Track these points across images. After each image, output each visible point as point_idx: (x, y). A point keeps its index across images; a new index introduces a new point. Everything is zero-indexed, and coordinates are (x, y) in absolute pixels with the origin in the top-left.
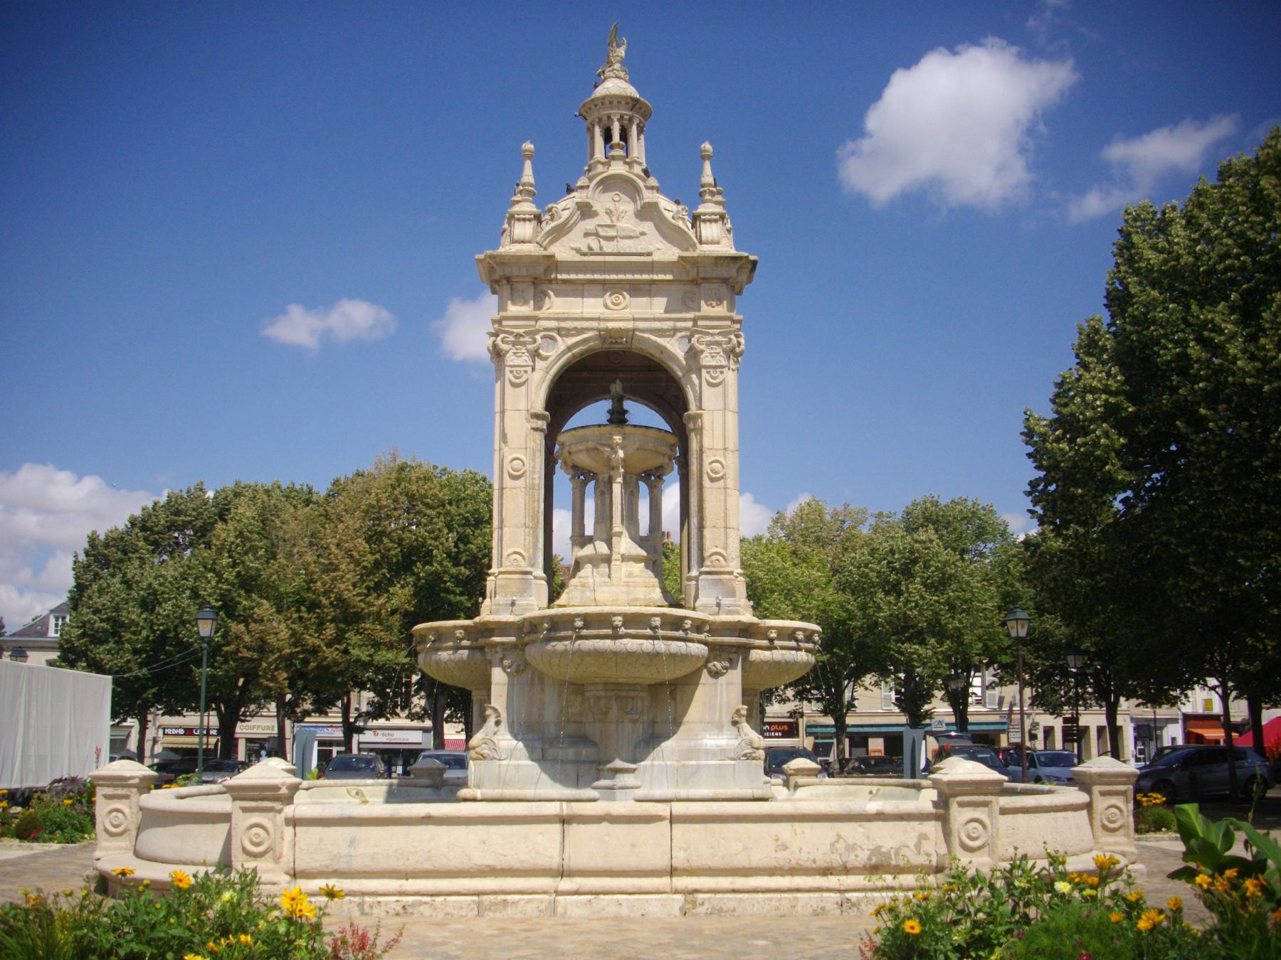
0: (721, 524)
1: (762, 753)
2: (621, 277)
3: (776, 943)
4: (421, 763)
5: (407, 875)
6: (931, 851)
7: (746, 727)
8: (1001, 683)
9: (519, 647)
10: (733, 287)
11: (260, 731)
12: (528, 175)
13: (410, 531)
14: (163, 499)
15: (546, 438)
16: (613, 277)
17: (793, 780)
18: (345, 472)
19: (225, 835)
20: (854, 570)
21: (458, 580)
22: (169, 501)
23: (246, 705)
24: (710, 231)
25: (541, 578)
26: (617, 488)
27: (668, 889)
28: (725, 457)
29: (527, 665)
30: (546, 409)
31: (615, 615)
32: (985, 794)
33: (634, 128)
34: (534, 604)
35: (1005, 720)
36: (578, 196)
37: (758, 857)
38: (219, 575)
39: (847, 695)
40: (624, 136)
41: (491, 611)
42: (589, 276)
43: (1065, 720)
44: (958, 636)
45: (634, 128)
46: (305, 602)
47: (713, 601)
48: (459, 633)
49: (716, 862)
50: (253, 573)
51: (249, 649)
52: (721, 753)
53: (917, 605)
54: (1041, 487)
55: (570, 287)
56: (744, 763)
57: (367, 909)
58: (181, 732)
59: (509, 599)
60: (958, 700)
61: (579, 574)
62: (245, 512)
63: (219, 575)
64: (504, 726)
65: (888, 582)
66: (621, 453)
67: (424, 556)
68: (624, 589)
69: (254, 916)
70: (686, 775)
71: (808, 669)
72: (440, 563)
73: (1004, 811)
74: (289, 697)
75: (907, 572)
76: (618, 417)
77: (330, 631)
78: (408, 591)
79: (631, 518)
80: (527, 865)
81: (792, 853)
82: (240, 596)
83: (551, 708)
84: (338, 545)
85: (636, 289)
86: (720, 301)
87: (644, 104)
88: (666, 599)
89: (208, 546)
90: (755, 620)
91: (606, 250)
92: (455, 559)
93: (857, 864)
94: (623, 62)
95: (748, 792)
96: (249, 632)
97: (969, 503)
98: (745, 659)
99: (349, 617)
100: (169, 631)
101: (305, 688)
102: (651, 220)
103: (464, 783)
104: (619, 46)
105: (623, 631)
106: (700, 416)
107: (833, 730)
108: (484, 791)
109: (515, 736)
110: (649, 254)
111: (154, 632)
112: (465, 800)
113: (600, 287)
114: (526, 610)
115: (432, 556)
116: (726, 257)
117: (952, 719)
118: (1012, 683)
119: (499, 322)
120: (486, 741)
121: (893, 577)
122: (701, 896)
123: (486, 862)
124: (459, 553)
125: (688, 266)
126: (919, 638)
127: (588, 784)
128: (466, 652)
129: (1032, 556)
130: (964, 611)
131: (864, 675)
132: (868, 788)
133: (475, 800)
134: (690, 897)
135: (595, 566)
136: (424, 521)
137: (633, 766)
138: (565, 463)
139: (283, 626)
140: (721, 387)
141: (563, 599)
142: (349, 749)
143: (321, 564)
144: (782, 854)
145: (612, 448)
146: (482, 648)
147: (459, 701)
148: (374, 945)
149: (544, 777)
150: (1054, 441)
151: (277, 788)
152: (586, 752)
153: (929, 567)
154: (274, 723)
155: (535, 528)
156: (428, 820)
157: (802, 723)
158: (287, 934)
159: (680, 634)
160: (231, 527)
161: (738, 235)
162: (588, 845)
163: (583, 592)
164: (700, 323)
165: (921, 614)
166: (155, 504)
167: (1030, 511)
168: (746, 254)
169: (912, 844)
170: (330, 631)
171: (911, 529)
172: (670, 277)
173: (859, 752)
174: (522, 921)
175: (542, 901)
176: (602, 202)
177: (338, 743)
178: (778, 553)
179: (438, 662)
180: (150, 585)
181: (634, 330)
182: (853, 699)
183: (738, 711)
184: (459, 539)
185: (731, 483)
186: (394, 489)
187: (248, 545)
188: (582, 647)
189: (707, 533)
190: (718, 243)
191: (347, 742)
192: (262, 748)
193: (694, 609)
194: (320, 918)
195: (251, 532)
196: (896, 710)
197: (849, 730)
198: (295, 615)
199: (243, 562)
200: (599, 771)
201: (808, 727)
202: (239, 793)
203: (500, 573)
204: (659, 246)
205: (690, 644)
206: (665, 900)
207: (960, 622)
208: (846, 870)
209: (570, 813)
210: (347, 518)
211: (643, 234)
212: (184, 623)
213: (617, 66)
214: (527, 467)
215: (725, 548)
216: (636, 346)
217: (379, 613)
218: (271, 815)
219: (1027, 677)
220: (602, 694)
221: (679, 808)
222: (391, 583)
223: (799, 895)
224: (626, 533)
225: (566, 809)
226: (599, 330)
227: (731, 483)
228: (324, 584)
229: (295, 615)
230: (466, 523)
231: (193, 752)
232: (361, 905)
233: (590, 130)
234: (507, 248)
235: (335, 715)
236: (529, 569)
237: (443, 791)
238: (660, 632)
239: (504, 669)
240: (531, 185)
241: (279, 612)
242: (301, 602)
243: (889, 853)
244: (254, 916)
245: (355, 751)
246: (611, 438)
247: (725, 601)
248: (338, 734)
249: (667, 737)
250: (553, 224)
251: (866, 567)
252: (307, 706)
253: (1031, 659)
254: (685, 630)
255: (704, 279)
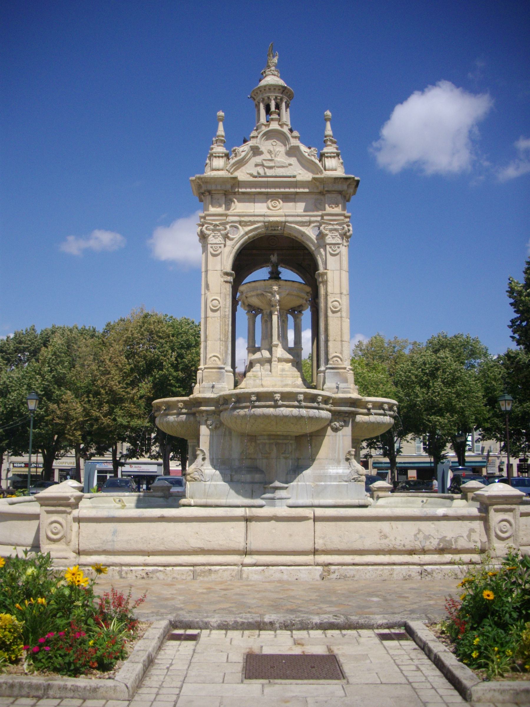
0: (339, 338)
1: (364, 478)
2: (277, 190)
3: (385, 600)
4: (156, 483)
5: (149, 554)
6: (477, 539)
7: (354, 462)
8: (483, 438)
9: (217, 413)
10: (345, 197)
11: (67, 465)
12: (221, 131)
13: (151, 352)
14: (12, 336)
15: (233, 287)
16: (273, 190)
17: (376, 494)
18: (114, 319)
19: (36, 528)
20: (403, 374)
21: (178, 380)
22: (16, 336)
23: (58, 450)
24: (330, 163)
25: (230, 372)
26: (275, 318)
27: (313, 564)
28: (341, 298)
29: (221, 424)
30: (233, 270)
31: (276, 393)
32: (512, 504)
33: (284, 104)
34: (226, 387)
35: (485, 460)
36: (251, 143)
37: (368, 544)
38: (43, 377)
39: (396, 446)
40: (278, 107)
41: (200, 391)
42: (258, 190)
43: (521, 460)
44: (461, 412)
45: (284, 104)
46: (91, 392)
47: (334, 385)
48: (180, 405)
49: (343, 546)
50: (61, 375)
51: (59, 418)
52: (338, 477)
53: (439, 394)
54: (518, 323)
55: (247, 197)
56: (353, 484)
57: (124, 574)
58: (23, 465)
59: (211, 384)
60: (460, 449)
61: (252, 370)
62: (57, 341)
63: (43, 377)
64: (207, 461)
65: (422, 381)
66: (278, 297)
67: (158, 366)
68: (280, 378)
69: (47, 585)
70: (319, 491)
71: (391, 427)
72: (167, 370)
73: (523, 515)
74: (82, 446)
75: (433, 375)
76: (275, 276)
77: (106, 408)
78: (150, 385)
79: (283, 337)
80: (224, 548)
81: (390, 540)
82: (54, 388)
83: (236, 449)
84: (110, 360)
85: (287, 198)
86: (337, 205)
87: (289, 90)
88: (305, 384)
89: (37, 360)
90: (360, 397)
91: (268, 174)
92: (176, 367)
93: (431, 548)
94: (276, 66)
95: (356, 502)
96: (60, 409)
97: (464, 337)
98: (353, 421)
99: (116, 400)
100: (15, 408)
101: (92, 440)
102: (295, 156)
103: (183, 495)
104: (274, 57)
105: (280, 403)
106: (326, 274)
107: (389, 465)
108: (196, 500)
109: (215, 467)
110: (294, 177)
111: (6, 408)
112: (184, 506)
113: (265, 197)
114: (221, 391)
115: (163, 366)
116: (341, 178)
117: (456, 459)
118: (490, 439)
119: (204, 218)
120: (197, 470)
121: (425, 378)
122: (333, 567)
123: (198, 546)
124: (178, 364)
125: (318, 184)
126: (440, 412)
127: (259, 497)
128: (184, 416)
129: (512, 363)
130: (465, 397)
131: (407, 434)
132: (421, 499)
133: (190, 506)
134: (326, 568)
135: (262, 365)
136: (158, 346)
137: (286, 485)
138: (244, 303)
139: (79, 405)
140: (338, 256)
141: (243, 385)
142: (116, 475)
143: (100, 370)
144: (384, 541)
145: (272, 294)
146: (194, 414)
147: (179, 447)
148: (127, 603)
149: (232, 492)
150: (526, 296)
151: (68, 498)
152: (257, 477)
153: (445, 373)
154: (74, 460)
155: (226, 342)
156: (162, 519)
157: (371, 461)
158: (70, 596)
159: (315, 405)
160: (50, 350)
161: (346, 165)
162: (262, 535)
163: (254, 380)
164: (325, 218)
165: (441, 399)
166: (8, 337)
167: (511, 337)
168: (353, 176)
169: (465, 535)
170: (106, 408)
171: (436, 351)
172: (307, 190)
173: (403, 478)
174: (221, 583)
175: (233, 570)
176: (265, 146)
177: (110, 472)
178: (359, 364)
179: (168, 423)
180: (5, 382)
181: (285, 222)
182: (400, 448)
183: (349, 452)
184: (178, 356)
185: (344, 314)
186: (141, 328)
187: (59, 359)
188: (256, 413)
189: (330, 344)
190: (336, 170)
191: (115, 471)
192: (68, 474)
193: (323, 390)
194: (91, 586)
195: (60, 352)
196: (424, 454)
197: (398, 465)
198: (86, 399)
199: (56, 370)
200: (265, 488)
201: (374, 463)
202: (44, 502)
203: (205, 368)
204: (300, 172)
205: (321, 411)
206: (310, 570)
207: (463, 403)
208: (424, 552)
209: (252, 515)
210: (114, 344)
211: (290, 165)
212: (23, 403)
213: (273, 68)
214: (221, 305)
215: (341, 353)
216: (286, 232)
217: (133, 398)
218: (64, 515)
219: (499, 436)
220: (267, 441)
221: (319, 512)
222: (140, 381)
223: (395, 567)
224: (280, 345)
225: (249, 512)
226: (264, 222)
227: (344, 314)
228: (102, 382)
229: (86, 399)
230: (182, 347)
231: (25, 476)
232: (120, 572)
233: (258, 106)
234: (209, 173)
235: (108, 456)
236: (223, 366)
237: (170, 499)
238: (303, 404)
239: (208, 427)
240: (223, 136)
241: (77, 398)
242: (88, 392)
243: (451, 541)
244: (47, 585)
245: (119, 476)
246: (272, 288)
247: (341, 385)
248: (110, 467)
249: (307, 467)
250: (236, 159)
251: (409, 372)
252: (93, 451)
253: (501, 425)
254: (318, 403)
255: (328, 192)
